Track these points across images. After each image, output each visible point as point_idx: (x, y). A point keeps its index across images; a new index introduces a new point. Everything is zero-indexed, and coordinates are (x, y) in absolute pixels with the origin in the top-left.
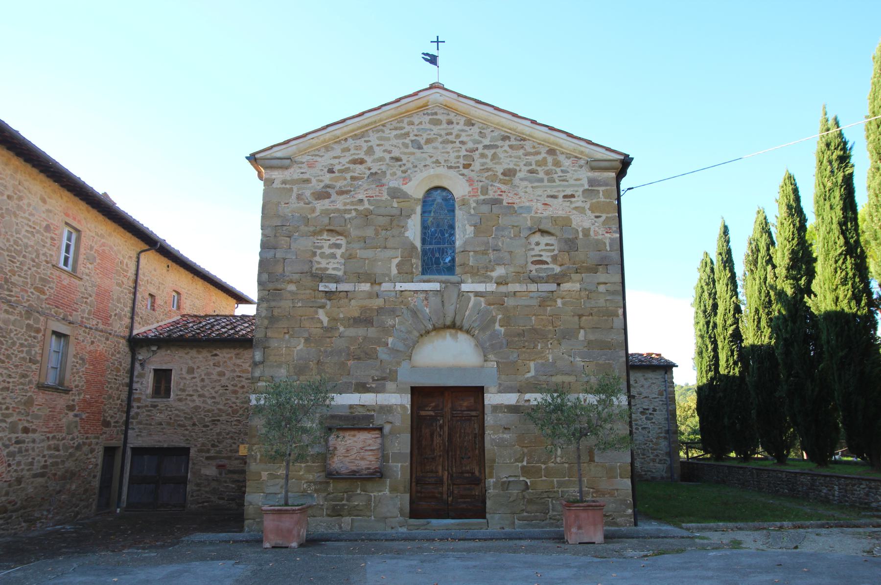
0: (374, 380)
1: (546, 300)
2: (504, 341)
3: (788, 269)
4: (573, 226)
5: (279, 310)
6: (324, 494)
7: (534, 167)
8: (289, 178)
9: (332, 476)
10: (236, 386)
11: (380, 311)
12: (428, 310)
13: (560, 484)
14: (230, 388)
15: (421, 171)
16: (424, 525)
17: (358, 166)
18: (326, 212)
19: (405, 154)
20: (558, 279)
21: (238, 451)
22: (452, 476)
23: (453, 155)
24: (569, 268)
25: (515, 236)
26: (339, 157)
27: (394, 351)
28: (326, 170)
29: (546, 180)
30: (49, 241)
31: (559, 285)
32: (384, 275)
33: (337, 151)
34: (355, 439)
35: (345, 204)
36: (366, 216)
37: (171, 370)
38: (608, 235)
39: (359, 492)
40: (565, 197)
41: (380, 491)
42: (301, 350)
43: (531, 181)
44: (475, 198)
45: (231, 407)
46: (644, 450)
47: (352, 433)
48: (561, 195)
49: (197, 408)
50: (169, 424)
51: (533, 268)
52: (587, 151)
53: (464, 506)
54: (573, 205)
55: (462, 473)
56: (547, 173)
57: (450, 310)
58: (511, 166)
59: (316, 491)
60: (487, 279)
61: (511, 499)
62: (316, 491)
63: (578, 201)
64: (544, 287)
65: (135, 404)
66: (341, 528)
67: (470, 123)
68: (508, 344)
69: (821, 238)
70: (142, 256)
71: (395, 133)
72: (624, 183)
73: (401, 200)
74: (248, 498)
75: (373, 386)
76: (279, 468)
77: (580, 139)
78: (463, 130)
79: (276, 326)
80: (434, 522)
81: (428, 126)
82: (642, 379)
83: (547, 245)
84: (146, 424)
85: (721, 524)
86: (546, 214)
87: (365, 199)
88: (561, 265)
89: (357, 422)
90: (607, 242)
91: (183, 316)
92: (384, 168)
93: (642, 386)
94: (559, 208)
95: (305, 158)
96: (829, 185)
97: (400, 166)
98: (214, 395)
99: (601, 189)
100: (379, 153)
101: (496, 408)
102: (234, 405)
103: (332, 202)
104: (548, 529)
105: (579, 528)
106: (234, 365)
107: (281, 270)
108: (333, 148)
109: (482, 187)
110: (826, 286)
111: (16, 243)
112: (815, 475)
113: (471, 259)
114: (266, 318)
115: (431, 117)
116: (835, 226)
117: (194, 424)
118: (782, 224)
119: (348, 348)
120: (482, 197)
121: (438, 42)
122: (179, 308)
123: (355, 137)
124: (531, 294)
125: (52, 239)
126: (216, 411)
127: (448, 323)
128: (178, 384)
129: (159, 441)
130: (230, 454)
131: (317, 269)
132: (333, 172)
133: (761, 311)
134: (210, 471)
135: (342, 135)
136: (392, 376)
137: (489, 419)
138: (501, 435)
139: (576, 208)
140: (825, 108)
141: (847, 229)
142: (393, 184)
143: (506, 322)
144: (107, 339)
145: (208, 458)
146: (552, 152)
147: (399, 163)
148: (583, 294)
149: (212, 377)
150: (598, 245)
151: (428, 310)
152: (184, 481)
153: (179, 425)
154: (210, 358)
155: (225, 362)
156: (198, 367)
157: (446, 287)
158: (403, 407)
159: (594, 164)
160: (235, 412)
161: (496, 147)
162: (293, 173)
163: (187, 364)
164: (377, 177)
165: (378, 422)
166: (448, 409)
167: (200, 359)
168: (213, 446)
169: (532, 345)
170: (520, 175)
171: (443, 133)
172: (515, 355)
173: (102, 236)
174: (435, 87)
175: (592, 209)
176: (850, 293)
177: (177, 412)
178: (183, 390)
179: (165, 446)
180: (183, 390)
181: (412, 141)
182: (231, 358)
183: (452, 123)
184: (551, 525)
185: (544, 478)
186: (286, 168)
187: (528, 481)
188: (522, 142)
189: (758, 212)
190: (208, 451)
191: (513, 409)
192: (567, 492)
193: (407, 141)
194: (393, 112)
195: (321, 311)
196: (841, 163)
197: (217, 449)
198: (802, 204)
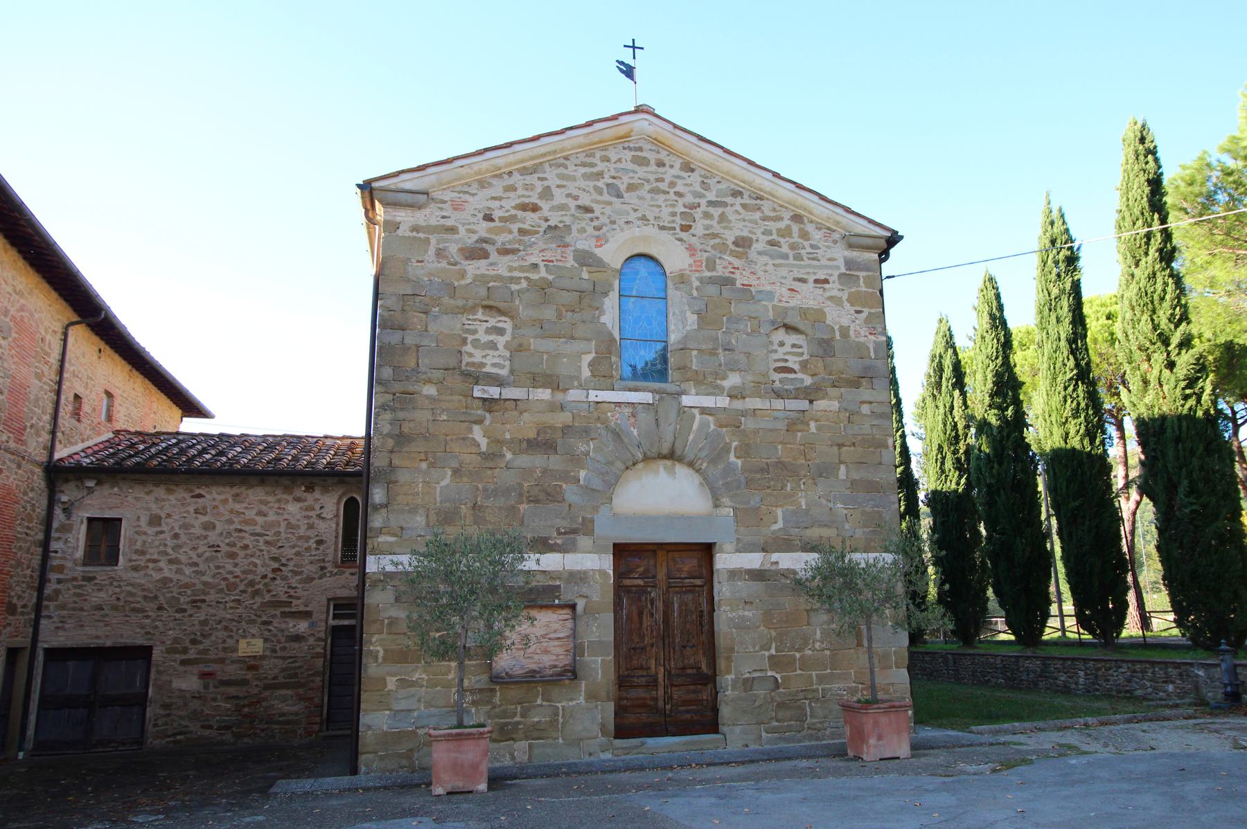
0: (559, 533)
1: (796, 422)
2: (742, 479)
3: (992, 396)
4: (828, 322)
5: (412, 425)
7: (775, 237)
8: (424, 224)
9: (498, 680)
10: (234, 545)
11: (566, 430)
12: (635, 432)
14: (224, 548)
15: (622, 230)
16: (637, 747)
17: (529, 215)
18: (481, 279)
19: (598, 202)
20: (811, 394)
21: (235, 650)
22: (670, 672)
23: (666, 211)
24: (823, 378)
26: (500, 199)
27: (589, 490)
28: (481, 216)
31: (811, 402)
32: (572, 378)
33: (497, 190)
36: (543, 288)
37: (120, 520)
38: (872, 338)
39: (539, 701)
40: (816, 281)
41: (572, 700)
42: (447, 486)
43: (772, 257)
45: (225, 579)
48: (811, 278)
49: (165, 581)
50: (115, 608)
51: (776, 377)
52: (844, 221)
53: (688, 716)
54: (828, 294)
55: (684, 668)
56: (793, 247)
57: (668, 432)
58: (745, 233)
59: (474, 703)
60: (716, 390)
61: (757, 704)
62: (474, 703)
63: (834, 289)
65: (53, 576)
66: (513, 758)
67: (688, 168)
68: (749, 483)
69: (1045, 358)
70: (72, 331)
71: (582, 170)
72: (887, 268)
73: (594, 269)
74: (365, 719)
75: (559, 541)
76: (415, 670)
77: (836, 204)
78: (678, 177)
79: (407, 449)
80: (651, 742)
81: (631, 166)
83: (794, 346)
84: (73, 609)
85: (1017, 724)
86: (793, 303)
87: (542, 264)
91: (117, 433)
92: (568, 220)
94: (809, 297)
95: (448, 196)
96: (1055, 292)
97: (592, 220)
98: (195, 559)
99: (862, 274)
100: (559, 197)
101: (734, 574)
102: (229, 576)
103: (491, 264)
104: (807, 743)
105: (880, 738)
106: (231, 511)
107: (412, 364)
108: (490, 185)
109: (708, 259)
110: (1053, 419)
112: (1048, 658)
113: (694, 360)
114: (389, 435)
116: (1063, 343)
117: (160, 608)
118: (983, 338)
119: (520, 484)
120: (708, 274)
121: (634, 47)
122: (109, 418)
123: (524, 171)
124: (776, 414)
126: (199, 586)
127: (665, 451)
128: (132, 542)
129: (97, 637)
130: (222, 655)
131: (467, 364)
132: (492, 220)
133: (946, 448)
134: (189, 683)
135: (506, 166)
136: (587, 528)
137: (723, 590)
138: (741, 613)
139: (831, 298)
140: (1048, 195)
141: (1077, 349)
142: (581, 245)
143: (744, 451)
144: (19, 466)
145: (183, 663)
146: (797, 218)
147: (590, 215)
149: (192, 531)
150: (860, 349)
151: (635, 432)
152: (141, 701)
153: (134, 610)
154: (189, 500)
155: (216, 507)
156: (169, 516)
157: (661, 399)
158: (603, 573)
160: (231, 587)
161: (725, 204)
162: (429, 216)
163: (148, 509)
164: (557, 233)
165: (567, 597)
166: (661, 575)
167: (173, 505)
168: (194, 642)
169: (780, 485)
170: (758, 246)
171: (652, 177)
172: (758, 499)
173: (20, 293)
174: (643, 111)
175: (852, 301)
176: (1083, 427)
177: (130, 588)
178: (143, 553)
179: (109, 643)
180: (143, 553)
181: (608, 185)
182: (225, 501)
183: (664, 165)
184: (811, 737)
185: (799, 672)
187: (778, 676)
188: (758, 202)
189: (941, 321)
190: (185, 650)
191: (757, 575)
192: (830, 689)
193: (600, 184)
194: (582, 140)
195: (476, 428)
196: (1069, 265)
197: (201, 647)
198: (1005, 313)
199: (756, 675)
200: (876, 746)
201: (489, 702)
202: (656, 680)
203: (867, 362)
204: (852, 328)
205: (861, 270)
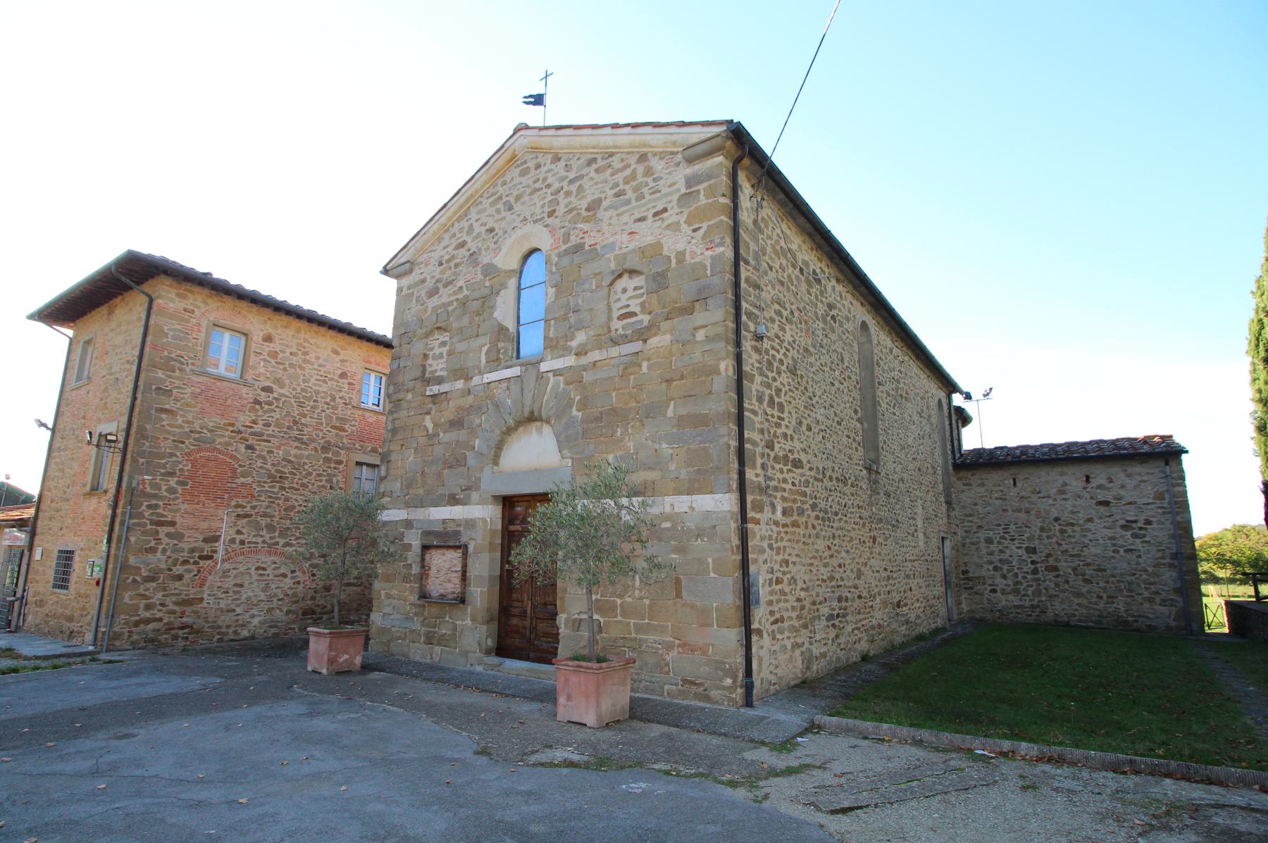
7: (622, 187)
13: (639, 629)
30: (346, 386)
31: (645, 341)
36: (463, 304)
38: (709, 253)
40: (655, 215)
46: (1130, 583)
54: (666, 223)
56: (636, 190)
57: (528, 400)
60: (566, 351)
62: (416, 614)
82: (1122, 476)
83: (636, 289)
85: (885, 726)
88: (650, 313)
93: (1123, 487)
94: (648, 233)
99: (701, 187)
100: (478, 229)
111: (302, 390)
120: (564, 247)
123: (459, 219)
125: (350, 384)
139: (668, 227)
143: (583, 406)
146: (643, 158)
148: (675, 348)
159: (688, 153)
165: (464, 540)
170: (605, 204)
171: (531, 182)
175: (688, 222)
185: (619, 618)
186: (411, 271)
192: (646, 641)
193: (500, 206)
195: (428, 417)
202: (525, 612)
205: (700, 182)
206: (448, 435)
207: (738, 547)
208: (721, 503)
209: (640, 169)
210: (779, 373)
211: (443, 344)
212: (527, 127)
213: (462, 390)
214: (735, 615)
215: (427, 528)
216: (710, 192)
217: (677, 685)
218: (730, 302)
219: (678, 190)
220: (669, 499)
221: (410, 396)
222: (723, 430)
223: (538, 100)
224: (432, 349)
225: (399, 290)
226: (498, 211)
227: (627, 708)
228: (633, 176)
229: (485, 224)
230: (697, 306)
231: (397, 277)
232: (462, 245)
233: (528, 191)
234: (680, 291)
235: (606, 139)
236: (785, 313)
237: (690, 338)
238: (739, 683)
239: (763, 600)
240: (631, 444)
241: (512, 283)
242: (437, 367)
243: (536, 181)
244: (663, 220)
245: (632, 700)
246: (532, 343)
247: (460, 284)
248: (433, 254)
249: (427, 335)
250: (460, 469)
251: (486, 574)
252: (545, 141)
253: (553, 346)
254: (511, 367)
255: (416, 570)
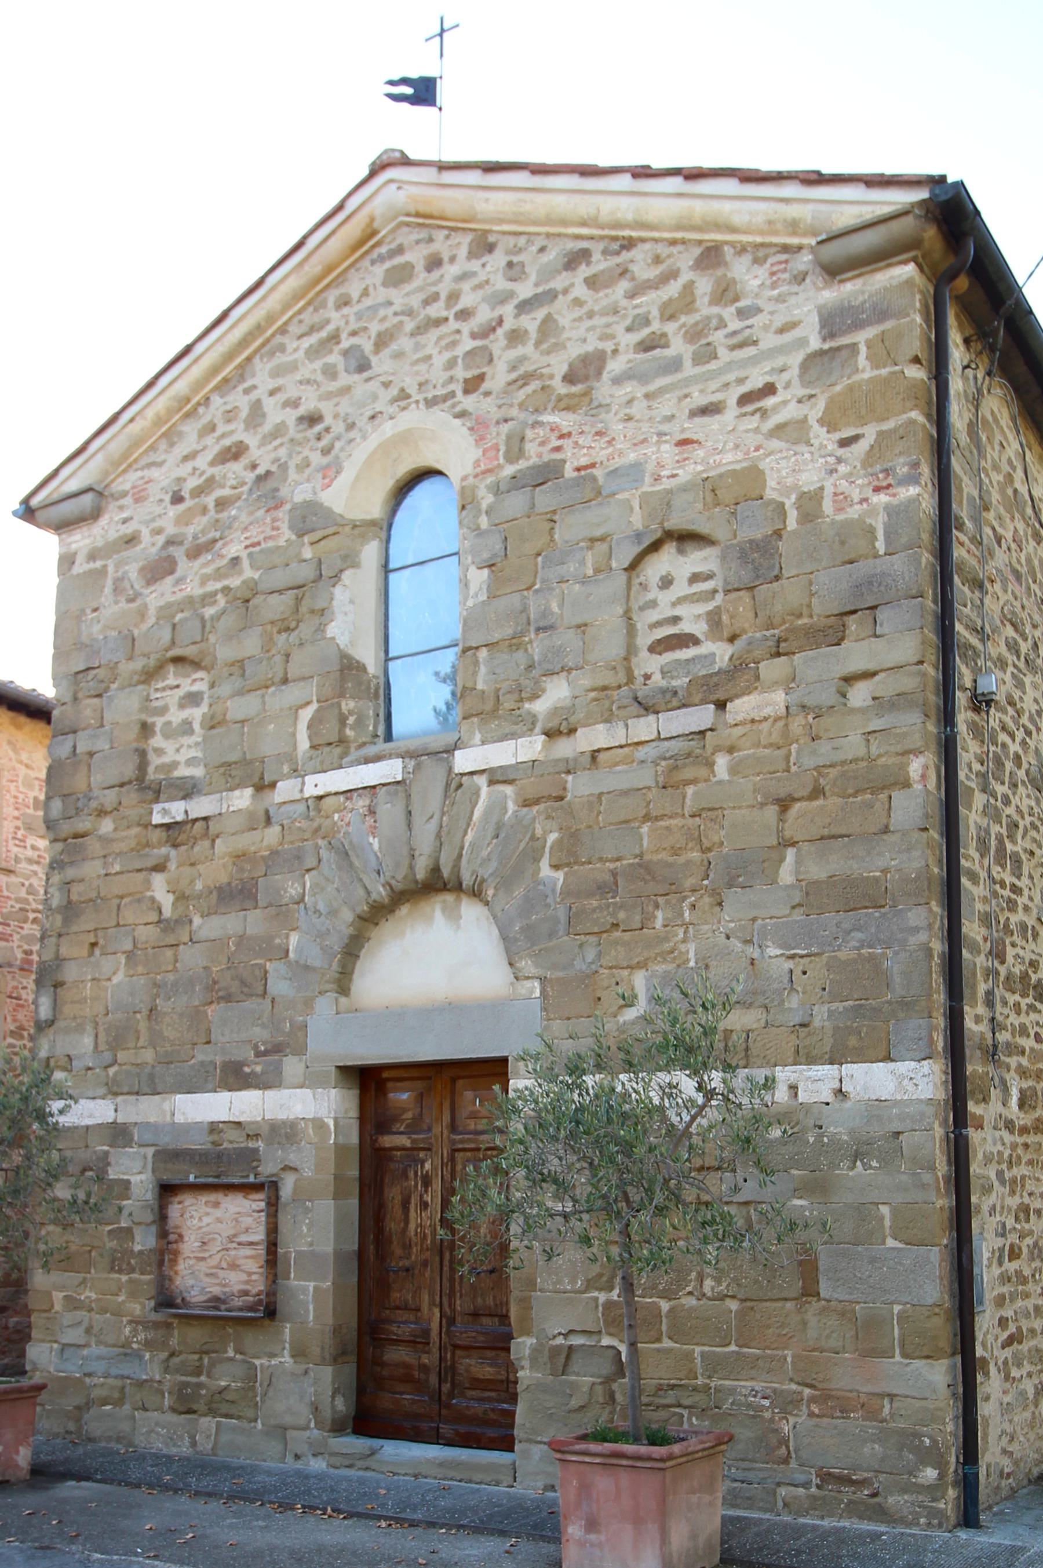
0: (259, 1054)
2: (562, 914)
4: (770, 494)
6: (164, 1355)
7: (656, 326)
8: (100, 543)
12: (375, 843)
23: (439, 360)
25: (597, 571)
28: (167, 498)
29: (687, 363)
31: (721, 706)
34: (218, 1213)
35: (204, 580)
36: (245, 600)
38: (882, 498)
40: (745, 399)
42: (119, 984)
44: (490, 479)
47: (213, 1197)
56: (694, 335)
58: (592, 345)
61: (574, 1403)
62: (148, 1344)
64: (680, 722)
66: (194, 1444)
75: (258, 1069)
77: (778, 177)
81: (382, 294)
83: (695, 578)
88: (732, 639)
89: (221, 1167)
90: (879, 524)
94: (726, 444)
99: (861, 337)
100: (275, 414)
115: (388, 265)
120: (510, 470)
123: (225, 386)
139: (779, 430)
142: (301, 494)
146: (711, 257)
148: (797, 725)
151: (375, 843)
157: (418, 767)
159: (835, 250)
164: (270, 484)
165: (268, 1169)
169: (636, 921)
170: (615, 366)
171: (415, 301)
172: (591, 954)
175: (829, 423)
185: (667, 1343)
186: (95, 515)
192: (732, 1391)
193: (334, 358)
195: (159, 881)
199: (577, 1341)
200: (581, 1544)
201: (164, 1344)
202: (426, 1333)
203: (864, 568)
204: (829, 490)
205: (859, 325)
206: (216, 921)
207: (947, 1179)
208: (906, 1082)
209: (704, 286)
210: (1014, 786)
211: (193, 699)
212: (405, 162)
213: (250, 814)
214: (942, 1329)
215: (166, 1141)
216: (883, 351)
217: (806, 1485)
218: (930, 618)
219: (803, 342)
220: (784, 1074)
221: (107, 826)
222: (916, 917)
223: (423, 92)
224: (163, 710)
225: (66, 561)
226: (330, 372)
227: (717, 1540)
228: (687, 301)
229: (295, 403)
230: (852, 622)
231: (61, 526)
232: (235, 453)
233: (410, 325)
234: (811, 586)
235: (616, 202)
236: (1024, 647)
237: (833, 699)
238: (950, 1477)
239: (989, 1296)
240: (691, 950)
241: (370, 553)
242: (180, 755)
243: (431, 299)
244: (764, 413)
245: (726, 1520)
246: (419, 703)
247: (234, 549)
248: (154, 473)
249: (149, 676)
250: (250, 1004)
251: (327, 1247)
252: (459, 197)
253: (478, 707)
254: (377, 758)
255: (144, 1241)
